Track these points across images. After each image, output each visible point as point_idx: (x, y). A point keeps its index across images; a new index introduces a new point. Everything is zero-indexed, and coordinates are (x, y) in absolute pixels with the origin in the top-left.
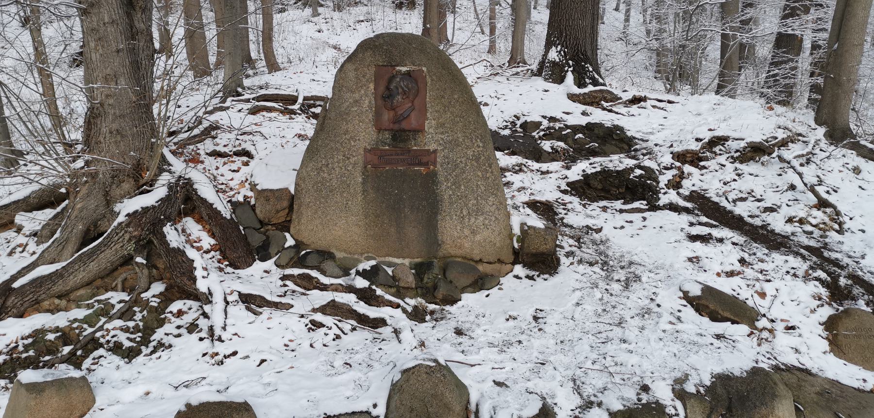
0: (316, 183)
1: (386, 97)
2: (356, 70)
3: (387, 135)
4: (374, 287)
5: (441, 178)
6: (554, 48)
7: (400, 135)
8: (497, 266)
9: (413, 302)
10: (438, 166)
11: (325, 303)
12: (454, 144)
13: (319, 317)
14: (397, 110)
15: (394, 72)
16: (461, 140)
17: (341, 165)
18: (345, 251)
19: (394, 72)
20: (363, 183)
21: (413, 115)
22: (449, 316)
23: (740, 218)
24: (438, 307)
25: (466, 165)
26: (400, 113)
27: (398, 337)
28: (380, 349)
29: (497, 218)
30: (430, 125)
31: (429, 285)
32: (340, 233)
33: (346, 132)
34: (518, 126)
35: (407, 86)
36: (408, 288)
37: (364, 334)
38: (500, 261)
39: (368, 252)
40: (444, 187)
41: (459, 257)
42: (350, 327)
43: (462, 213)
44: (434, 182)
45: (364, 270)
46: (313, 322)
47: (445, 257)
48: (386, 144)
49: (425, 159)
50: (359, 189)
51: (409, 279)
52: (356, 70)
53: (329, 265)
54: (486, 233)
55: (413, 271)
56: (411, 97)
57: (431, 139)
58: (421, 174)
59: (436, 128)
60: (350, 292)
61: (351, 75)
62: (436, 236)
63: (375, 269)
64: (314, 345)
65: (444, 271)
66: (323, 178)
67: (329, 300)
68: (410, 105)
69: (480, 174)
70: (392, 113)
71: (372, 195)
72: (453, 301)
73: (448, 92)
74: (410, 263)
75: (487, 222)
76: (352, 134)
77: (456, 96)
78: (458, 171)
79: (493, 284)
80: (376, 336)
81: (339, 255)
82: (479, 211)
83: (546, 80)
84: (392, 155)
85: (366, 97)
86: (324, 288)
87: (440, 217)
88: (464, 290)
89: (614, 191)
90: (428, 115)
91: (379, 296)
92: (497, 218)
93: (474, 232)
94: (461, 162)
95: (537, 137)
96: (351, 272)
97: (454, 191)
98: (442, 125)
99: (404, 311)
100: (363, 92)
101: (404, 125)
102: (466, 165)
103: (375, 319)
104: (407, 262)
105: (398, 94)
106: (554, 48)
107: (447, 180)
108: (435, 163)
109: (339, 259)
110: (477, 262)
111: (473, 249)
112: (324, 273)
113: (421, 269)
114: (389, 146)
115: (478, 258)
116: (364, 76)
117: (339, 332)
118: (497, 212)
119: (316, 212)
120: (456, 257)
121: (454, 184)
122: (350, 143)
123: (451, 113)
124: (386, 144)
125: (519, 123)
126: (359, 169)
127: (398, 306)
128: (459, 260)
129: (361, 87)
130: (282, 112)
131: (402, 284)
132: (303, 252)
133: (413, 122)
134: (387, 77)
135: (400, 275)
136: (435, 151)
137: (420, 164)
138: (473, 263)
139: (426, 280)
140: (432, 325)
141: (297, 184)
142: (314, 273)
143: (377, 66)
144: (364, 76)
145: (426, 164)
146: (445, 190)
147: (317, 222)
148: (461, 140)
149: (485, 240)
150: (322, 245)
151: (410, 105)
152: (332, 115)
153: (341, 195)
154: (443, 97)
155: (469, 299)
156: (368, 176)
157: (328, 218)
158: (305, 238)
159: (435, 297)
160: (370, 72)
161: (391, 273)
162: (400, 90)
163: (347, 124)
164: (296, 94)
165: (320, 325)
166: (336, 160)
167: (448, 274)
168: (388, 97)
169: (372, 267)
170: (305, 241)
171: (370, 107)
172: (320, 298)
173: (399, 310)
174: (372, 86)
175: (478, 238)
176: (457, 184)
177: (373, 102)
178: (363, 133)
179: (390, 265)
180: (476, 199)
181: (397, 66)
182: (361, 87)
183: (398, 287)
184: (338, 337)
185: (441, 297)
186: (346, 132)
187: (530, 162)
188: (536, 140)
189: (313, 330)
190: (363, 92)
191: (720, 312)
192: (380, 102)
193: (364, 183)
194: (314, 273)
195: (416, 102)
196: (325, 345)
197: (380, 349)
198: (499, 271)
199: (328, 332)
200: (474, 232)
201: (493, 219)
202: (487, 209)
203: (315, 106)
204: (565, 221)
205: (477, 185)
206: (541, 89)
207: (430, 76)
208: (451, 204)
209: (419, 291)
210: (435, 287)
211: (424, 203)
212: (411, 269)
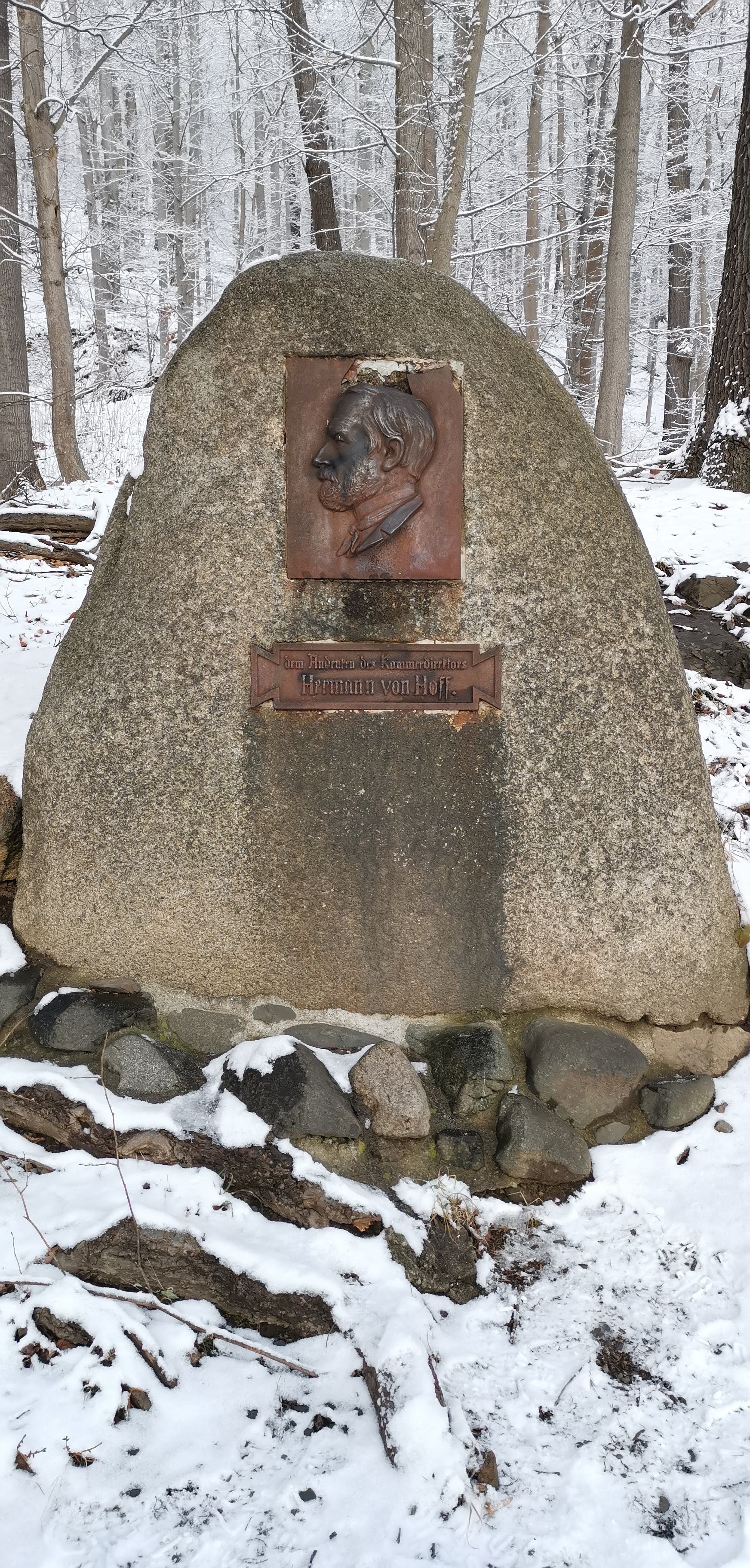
0: (89, 764)
1: (325, 464)
2: (221, 371)
3: (330, 598)
4: (284, 1146)
5: (515, 745)
6: (731, 405)
7: (376, 596)
8: (698, 1036)
9: (424, 1198)
10: (506, 703)
11: (95, 1231)
12: (560, 626)
13: (69, 1298)
14: (362, 508)
15: (353, 378)
16: (582, 613)
17: (170, 702)
18: (190, 988)
19: (353, 378)
20: (247, 765)
21: (418, 527)
22: (561, 1256)
24: (512, 1210)
25: (600, 698)
26: (372, 519)
27: (393, 1462)
28: (308, 1495)
30: (475, 562)
31: (481, 1120)
32: (173, 930)
33: (190, 588)
34: (671, 590)
35: (398, 426)
36: (405, 1141)
37: (244, 1376)
38: (707, 1020)
39: (266, 994)
40: (524, 776)
41: (574, 1010)
42: (187, 1341)
43: (584, 861)
44: (490, 757)
45: (250, 1073)
46: (43, 1319)
47: (525, 1012)
48: (324, 628)
49: (459, 682)
50: (235, 783)
51: (409, 1106)
52: (221, 371)
53: (134, 1053)
54: (665, 929)
55: (421, 1067)
56: (412, 464)
57: (481, 610)
58: (448, 731)
59: (500, 573)
60: (199, 1162)
61: (205, 389)
62: (496, 939)
63: (292, 1073)
64: (32, 1462)
65: (528, 1064)
66: (111, 747)
67: (114, 1219)
68: (408, 490)
69: (644, 728)
70: (345, 521)
71: (277, 804)
72: (564, 1183)
73: (539, 448)
74: (410, 1034)
75: (666, 891)
76: (209, 597)
77: (563, 464)
78: (572, 719)
79: (696, 1107)
80: (291, 1386)
81: (169, 1002)
82: (640, 856)
83: (712, 482)
84: (346, 667)
85: (258, 464)
86: (105, 1144)
87: (509, 878)
88: (595, 1133)
90: (472, 527)
91: (302, 1185)
93: (623, 927)
94: (583, 688)
95: (728, 616)
96: (208, 1070)
98: (520, 562)
99: (399, 1250)
100: (244, 448)
101: (387, 563)
102: (600, 698)
103: (287, 1300)
104: (393, 1029)
105: (368, 452)
106: (731, 405)
107: (536, 751)
108: (493, 696)
109: (169, 1018)
110: (631, 1025)
111: (622, 984)
112: (111, 1081)
113: (449, 1057)
114: (336, 634)
115: (637, 1014)
116: (247, 394)
117: (141, 1377)
118: (698, 857)
119: (91, 862)
120: (563, 1009)
121: (558, 764)
122: (201, 626)
123: (549, 519)
124: (324, 628)
125: (672, 583)
126: (234, 715)
127: (373, 1227)
128: (575, 1019)
129: (240, 431)
130: (48, 559)
131: (386, 1128)
132: (48, 998)
133: (419, 550)
134: (326, 395)
135: (377, 1090)
136: (495, 653)
137: (443, 697)
138: (620, 1030)
139: (466, 1103)
140: (503, 1313)
141: (30, 768)
142: (76, 1084)
143: (294, 357)
144: (247, 394)
145: (465, 698)
146: (529, 785)
147: (98, 892)
148: (582, 613)
149: (660, 953)
150: (110, 966)
151: (408, 490)
152: (143, 532)
153: (175, 806)
154: (521, 465)
155: (623, 1169)
156: (264, 739)
157: (132, 880)
158: (57, 943)
159: (502, 1172)
160: (270, 379)
161: (344, 1083)
162: (375, 440)
163: (191, 561)
164: (90, 514)
165: (74, 1336)
166: (153, 685)
167: (542, 1079)
168: (333, 466)
169: (280, 1064)
170: (57, 953)
171: (269, 499)
172: (86, 1195)
173: (378, 1245)
174: (275, 428)
175: (639, 944)
176: (567, 765)
177: (281, 484)
178: (246, 593)
179: (344, 1041)
180: (632, 813)
181: (363, 356)
182: (240, 431)
183: (371, 1137)
184: (138, 1400)
185: (522, 1169)
186: (190, 588)
187: (721, 687)
188: (726, 627)
189: (44, 1357)
190: (244, 448)
192: (305, 484)
193: (251, 762)
194: (76, 1084)
195: (428, 482)
196: (79, 1461)
197: (308, 1495)
198: (708, 1055)
199: (100, 1376)
200: (623, 927)
201: (688, 879)
202: (667, 845)
205: (636, 768)
206: (705, 504)
207: (478, 393)
209: (446, 1145)
210: (502, 1135)
211: (458, 831)
212: (412, 1058)
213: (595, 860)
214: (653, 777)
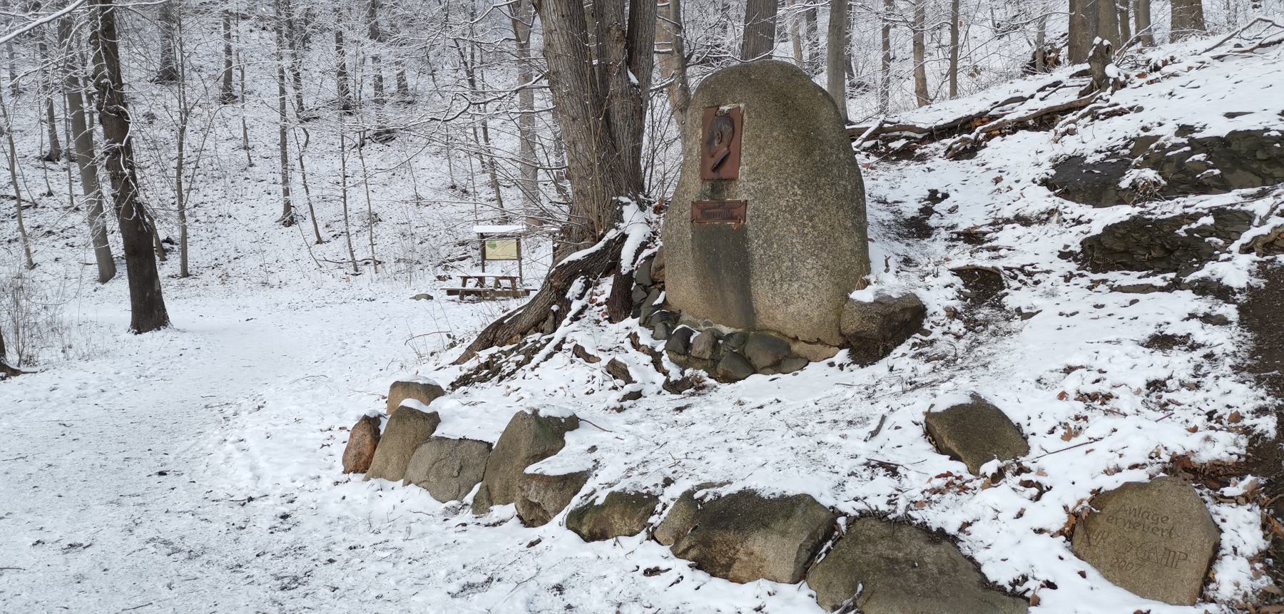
5: (751, 235)
10: (748, 220)
12: (766, 192)
23: (98, 253)
29: (815, 287)
40: (755, 245)
54: (801, 305)
59: (749, 175)
69: (794, 229)
73: (767, 129)
78: (769, 225)
82: (793, 276)
89: (1141, 255)
92: (815, 287)
97: (765, 250)
107: (758, 237)
128: (774, 334)
137: (732, 218)
146: (756, 247)
154: (759, 137)
175: (791, 309)
180: (791, 260)
185: (721, 372)
191: (945, 439)
200: (787, 302)
203: (898, 138)
204: (1004, 299)
208: (763, 265)
213: (777, 276)
214: (799, 247)
